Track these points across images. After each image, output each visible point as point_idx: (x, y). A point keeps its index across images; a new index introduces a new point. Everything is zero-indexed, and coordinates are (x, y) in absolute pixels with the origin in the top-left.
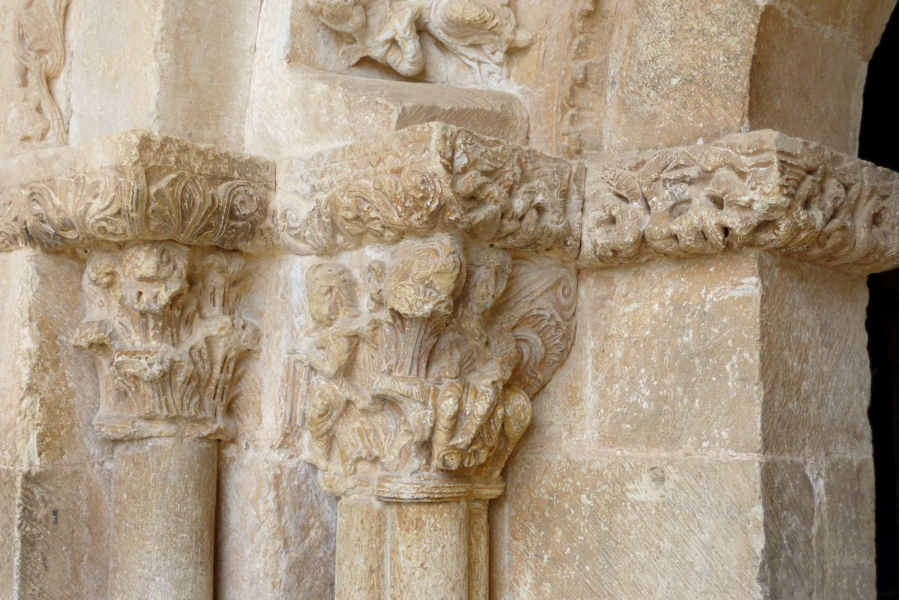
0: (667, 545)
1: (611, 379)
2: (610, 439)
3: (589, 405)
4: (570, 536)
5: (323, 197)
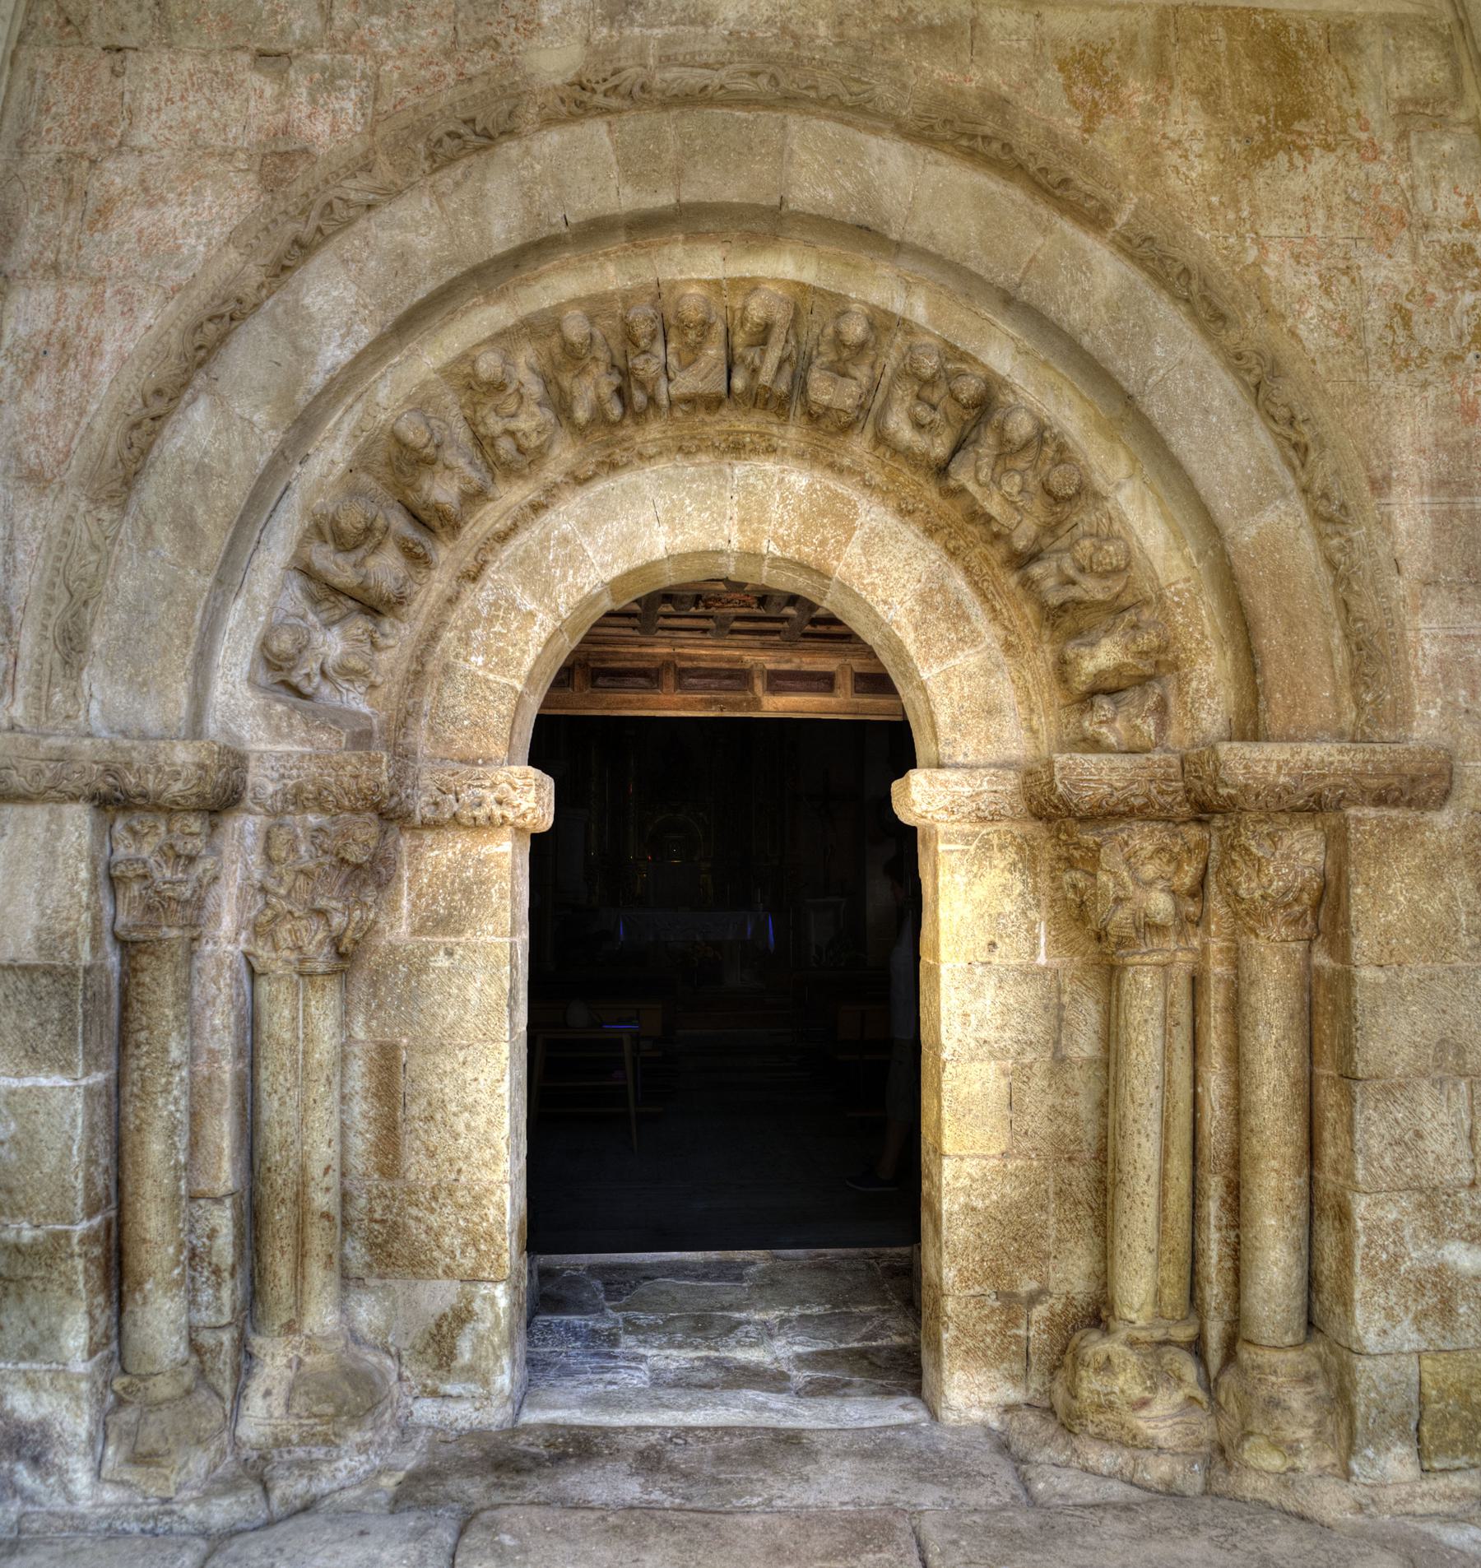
0: (455, 991)
1: (419, 896)
2: (417, 931)
3: (405, 912)
4: (390, 991)
5: (290, 783)
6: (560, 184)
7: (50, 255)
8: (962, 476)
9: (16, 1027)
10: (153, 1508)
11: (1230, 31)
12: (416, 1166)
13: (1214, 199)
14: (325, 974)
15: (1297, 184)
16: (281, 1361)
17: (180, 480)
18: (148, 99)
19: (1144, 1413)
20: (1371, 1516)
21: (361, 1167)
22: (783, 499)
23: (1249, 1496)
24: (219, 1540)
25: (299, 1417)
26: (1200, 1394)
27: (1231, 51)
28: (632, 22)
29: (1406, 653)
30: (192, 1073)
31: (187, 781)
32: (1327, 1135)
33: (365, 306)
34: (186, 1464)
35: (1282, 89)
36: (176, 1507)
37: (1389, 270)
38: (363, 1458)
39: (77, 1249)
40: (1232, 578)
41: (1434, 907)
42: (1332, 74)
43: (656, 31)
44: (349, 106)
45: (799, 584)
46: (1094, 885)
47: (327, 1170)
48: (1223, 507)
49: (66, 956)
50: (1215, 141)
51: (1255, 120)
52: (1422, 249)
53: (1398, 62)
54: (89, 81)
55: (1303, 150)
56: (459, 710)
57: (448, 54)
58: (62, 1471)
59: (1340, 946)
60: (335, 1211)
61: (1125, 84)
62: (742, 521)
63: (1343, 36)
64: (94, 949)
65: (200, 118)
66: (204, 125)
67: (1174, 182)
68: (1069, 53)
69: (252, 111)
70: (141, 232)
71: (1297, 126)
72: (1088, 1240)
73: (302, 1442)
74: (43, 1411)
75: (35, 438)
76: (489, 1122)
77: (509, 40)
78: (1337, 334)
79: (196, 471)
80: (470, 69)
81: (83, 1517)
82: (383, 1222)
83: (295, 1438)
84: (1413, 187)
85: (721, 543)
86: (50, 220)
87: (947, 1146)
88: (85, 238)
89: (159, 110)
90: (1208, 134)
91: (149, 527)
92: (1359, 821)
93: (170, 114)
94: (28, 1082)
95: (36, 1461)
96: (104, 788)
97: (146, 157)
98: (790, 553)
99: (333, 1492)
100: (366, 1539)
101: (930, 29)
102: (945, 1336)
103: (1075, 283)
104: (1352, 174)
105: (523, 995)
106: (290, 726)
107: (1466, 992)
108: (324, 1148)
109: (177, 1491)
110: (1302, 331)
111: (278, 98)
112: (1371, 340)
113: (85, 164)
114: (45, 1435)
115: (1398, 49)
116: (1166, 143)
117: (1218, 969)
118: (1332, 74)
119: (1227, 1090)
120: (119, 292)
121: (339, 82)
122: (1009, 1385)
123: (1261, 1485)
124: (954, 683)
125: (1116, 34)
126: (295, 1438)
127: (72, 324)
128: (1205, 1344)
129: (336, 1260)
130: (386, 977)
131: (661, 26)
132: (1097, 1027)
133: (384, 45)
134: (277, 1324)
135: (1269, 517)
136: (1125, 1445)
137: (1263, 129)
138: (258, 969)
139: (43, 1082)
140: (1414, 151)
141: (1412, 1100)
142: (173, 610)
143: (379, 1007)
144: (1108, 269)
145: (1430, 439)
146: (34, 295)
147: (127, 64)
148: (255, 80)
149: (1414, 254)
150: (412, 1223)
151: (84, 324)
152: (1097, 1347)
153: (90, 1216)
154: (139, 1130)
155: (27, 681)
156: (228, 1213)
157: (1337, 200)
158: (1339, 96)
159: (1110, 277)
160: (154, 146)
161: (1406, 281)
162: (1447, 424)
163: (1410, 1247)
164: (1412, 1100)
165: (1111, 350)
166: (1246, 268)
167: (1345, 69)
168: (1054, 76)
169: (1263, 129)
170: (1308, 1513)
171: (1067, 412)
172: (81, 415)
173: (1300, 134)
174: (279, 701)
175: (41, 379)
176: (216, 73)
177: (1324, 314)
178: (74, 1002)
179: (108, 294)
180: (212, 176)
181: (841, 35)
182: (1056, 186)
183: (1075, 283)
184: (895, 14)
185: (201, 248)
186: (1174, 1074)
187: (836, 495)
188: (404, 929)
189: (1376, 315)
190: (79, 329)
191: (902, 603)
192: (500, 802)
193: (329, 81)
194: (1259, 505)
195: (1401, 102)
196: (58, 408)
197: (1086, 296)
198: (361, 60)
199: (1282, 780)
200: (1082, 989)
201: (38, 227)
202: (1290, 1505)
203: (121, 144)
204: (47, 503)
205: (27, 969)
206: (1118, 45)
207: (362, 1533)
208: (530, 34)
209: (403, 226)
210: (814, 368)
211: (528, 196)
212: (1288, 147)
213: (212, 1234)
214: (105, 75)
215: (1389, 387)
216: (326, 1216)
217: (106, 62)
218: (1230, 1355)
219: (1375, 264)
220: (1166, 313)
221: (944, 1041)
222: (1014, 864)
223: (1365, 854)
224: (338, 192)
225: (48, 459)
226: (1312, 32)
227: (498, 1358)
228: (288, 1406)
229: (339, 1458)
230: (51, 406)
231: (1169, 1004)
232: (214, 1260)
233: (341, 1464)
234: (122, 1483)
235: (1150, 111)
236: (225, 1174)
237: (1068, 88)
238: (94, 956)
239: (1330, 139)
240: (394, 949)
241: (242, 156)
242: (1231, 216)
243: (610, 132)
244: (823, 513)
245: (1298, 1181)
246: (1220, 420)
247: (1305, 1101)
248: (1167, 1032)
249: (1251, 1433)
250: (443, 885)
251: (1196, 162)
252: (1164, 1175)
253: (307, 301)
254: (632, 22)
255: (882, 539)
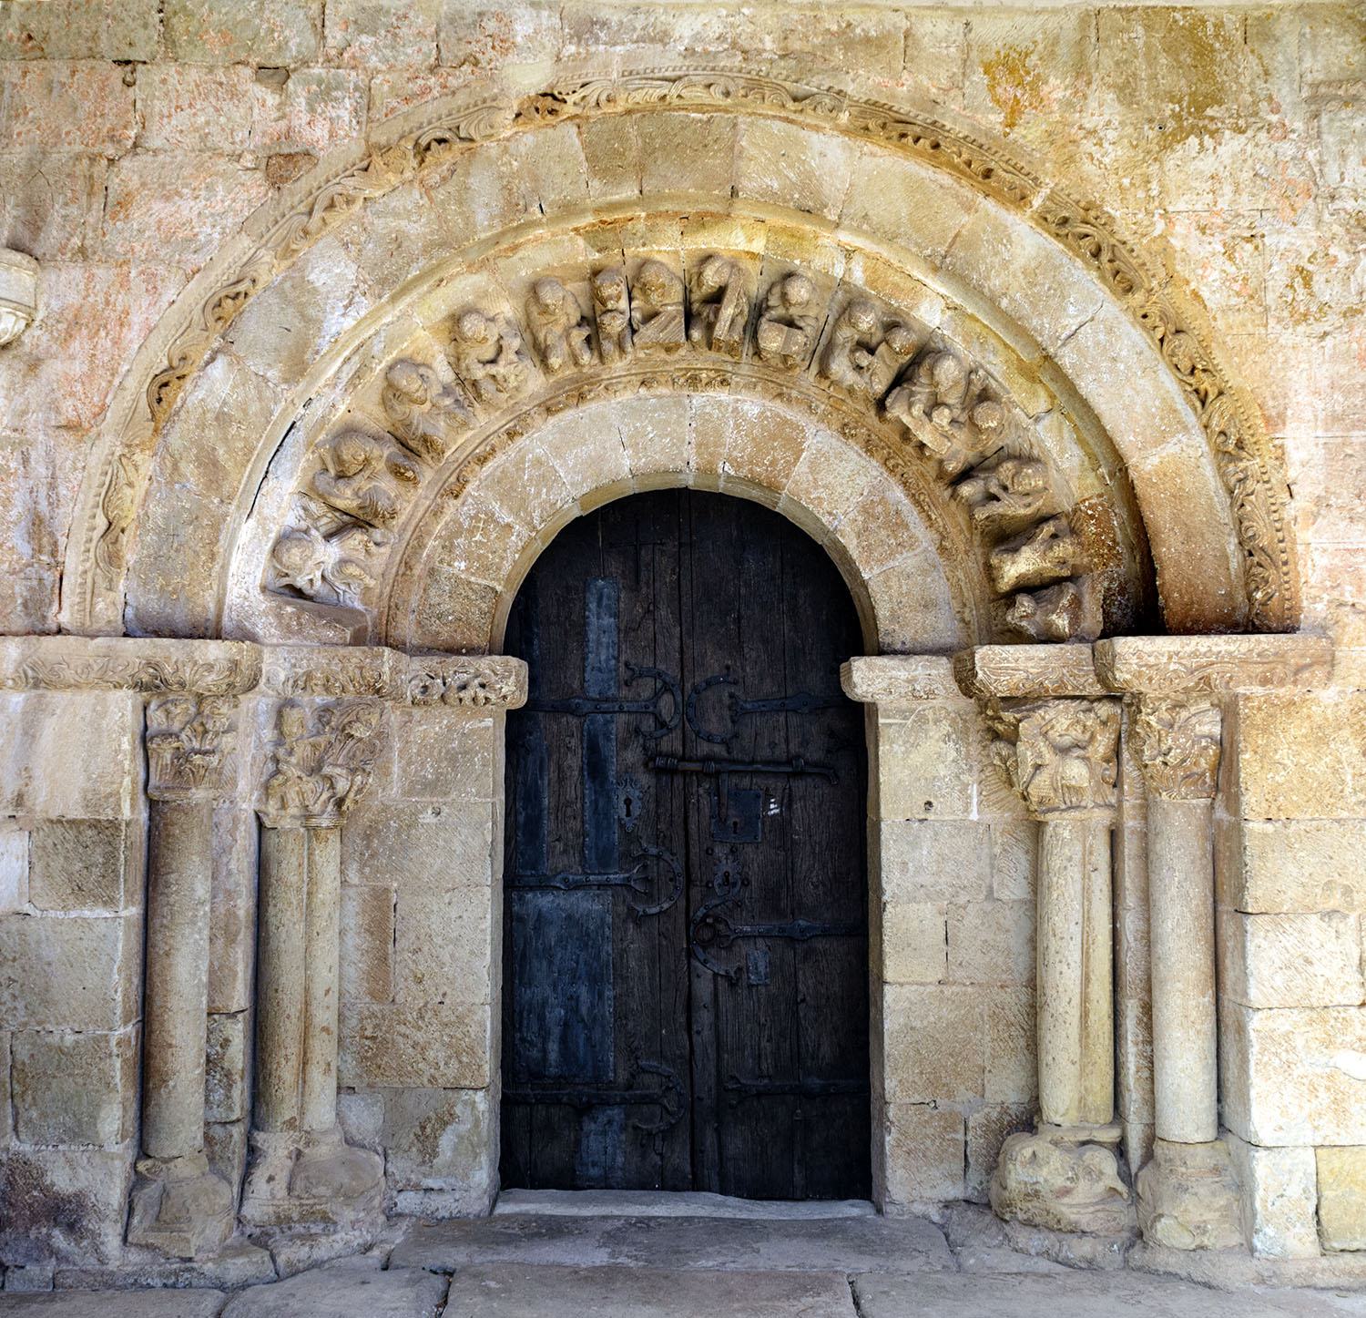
0: (441, 843)
1: (409, 764)
2: (409, 792)
4: (382, 843)
6: (535, 179)
7: (76, 241)
8: (897, 411)
9: (63, 869)
10: (174, 1266)
11: (1148, 28)
12: (405, 992)
13: (1126, 182)
14: (328, 828)
15: (1207, 164)
16: (282, 1153)
17: (202, 426)
18: (159, 106)
19: (1066, 1200)
20: (1273, 1287)
21: (353, 991)
22: (737, 426)
23: (1162, 1270)
24: (231, 1290)
25: (299, 1198)
26: (1121, 1187)
27: (1148, 45)
28: (597, 41)
29: (1296, 564)
30: (212, 910)
31: (220, 672)
32: (1228, 962)
33: (365, 282)
34: (203, 1231)
35: (1195, 82)
36: (195, 1265)
37: (1293, 239)
38: (357, 1233)
39: (115, 1051)
40: (1135, 497)
41: (1320, 768)
42: (1248, 65)
43: (618, 48)
44: (346, 116)
45: (754, 494)
46: (1015, 753)
47: (327, 992)
48: (1127, 441)
49: (110, 812)
50: (1129, 130)
51: (1169, 108)
52: (1326, 217)
53: (1314, 49)
54: (102, 89)
55: (1212, 134)
56: (444, 607)
57: (432, 70)
58: (95, 1235)
59: (1234, 803)
60: (334, 1028)
61: (1046, 82)
62: (699, 445)
63: (1258, 30)
64: (133, 806)
65: (208, 123)
66: (213, 129)
67: (1088, 168)
68: (993, 56)
69: (256, 117)
70: (160, 221)
71: (1209, 112)
72: (1021, 1056)
73: (303, 1218)
74: (79, 1185)
75: (72, 394)
76: (472, 952)
77: (487, 56)
78: (1238, 294)
79: (217, 419)
80: (453, 82)
81: (112, 1274)
82: (373, 1038)
83: (295, 1216)
84: (1321, 163)
85: (681, 464)
86: (74, 211)
87: (889, 974)
88: (109, 226)
89: (170, 116)
90: (1122, 123)
91: (175, 467)
92: (1247, 698)
93: (180, 119)
94: (73, 914)
95: (72, 1228)
96: (146, 678)
97: (161, 157)
98: (744, 472)
99: (331, 1259)
100: (366, 1286)
101: (867, 40)
102: (888, 1138)
103: (996, 254)
104: (1261, 154)
105: (501, 847)
106: (300, 624)
107: (1353, 841)
108: (325, 973)
109: (197, 1251)
110: (1205, 293)
111: (280, 107)
112: (1271, 298)
113: (105, 162)
114: (81, 1205)
115: (1314, 36)
116: (1081, 133)
117: (1131, 823)
118: (1248, 65)
119: (1141, 926)
120: (142, 272)
121: (334, 94)
122: (949, 1183)
123: (1172, 1260)
124: (894, 582)
125: (1039, 37)
126: (295, 1216)
127: (101, 298)
128: (1127, 1145)
129: (333, 1068)
130: (379, 832)
131: (624, 43)
132: (1027, 874)
133: (374, 61)
134: (280, 1120)
135: (1171, 449)
136: (1051, 1230)
137: (1177, 117)
138: (268, 824)
139: (87, 913)
140: (1325, 129)
141: (1301, 931)
142: (199, 532)
143: (372, 856)
144: (1026, 240)
145: (1326, 382)
146: (64, 275)
147: (137, 75)
148: (259, 90)
149: (1319, 221)
150: (400, 1039)
151: (112, 299)
152: (1024, 1148)
153: (126, 1023)
154: (167, 954)
155: (73, 592)
156: (240, 1026)
157: (1246, 175)
158: (1252, 82)
159: (1029, 249)
160: (167, 146)
161: (1309, 247)
162: (1343, 369)
163: (1302, 1055)
164: (1301, 931)
165: (1027, 308)
166: (1154, 240)
167: (1260, 58)
168: (979, 77)
169: (1177, 117)
170: (1214, 1283)
171: (992, 358)
172: (113, 375)
173: (1212, 119)
174: (289, 604)
175: (75, 346)
176: (221, 84)
177: (1228, 280)
178: (117, 849)
179: (133, 274)
180: (223, 174)
181: (785, 48)
182: (987, 172)
183: (996, 254)
184: (834, 28)
185: (216, 236)
186: (1093, 912)
187: (785, 421)
188: (395, 791)
189: (1279, 275)
190: (107, 303)
191: (846, 514)
192: (483, 686)
193: (325, 93)
194: (1162, 438)
195: (1315, 86)
196: (92, 370)
197: (1005, 264)
198: (353, 73)
199: (1172, 667)
200: (1013, 841)
201: (65, 217)
202: (1197, 1276)
203: (135, 145)
204: (85, 448)
205: (72, 822)
206: (1040, 47)
207: (363, 1283)
208: (505, 52)
209: (396, 215)
210: (763, 320)
211: (507, 188)
212: (1200, 132)
213: (226, 1043)
214: (119, 85)
215: (1287, 338)
216: (326, 1030)
217: (118, 72)
218: (1149, 1156)
219: (1279, 232)
220: (1084, 279)
221: (884, 885)
222: (948, 735)
223: (1253, 726)
224: (339, 189)
225: (86, 413)
226: (1229, 26)
227: (476, 1156)
228: (290, 1189)
229: (335, 1232)
230: (85, 368)
231: (1088, 852)
232: (226, 1065)
233: (337, 1237)
234: (149, 1247)
235: (1068, 105)
236: (239, 997)
237: (992, 88)
238: (132, 812)
239: (1242, 122)
240: (386, 808)
241: (250, 157)
242: (1141, 194)
243: (580, 133)
244: (773, 438)
245: (1201, 1000)
246: (1128, 368)
247: (1210, 933)
248: (1086, 877)
249: (1161, 1216)
250: (431, 755)
251: (1110, 148)
252: (1085, 999)
253: (312, 277)
254: (597, 41)
255: (827, 460)
